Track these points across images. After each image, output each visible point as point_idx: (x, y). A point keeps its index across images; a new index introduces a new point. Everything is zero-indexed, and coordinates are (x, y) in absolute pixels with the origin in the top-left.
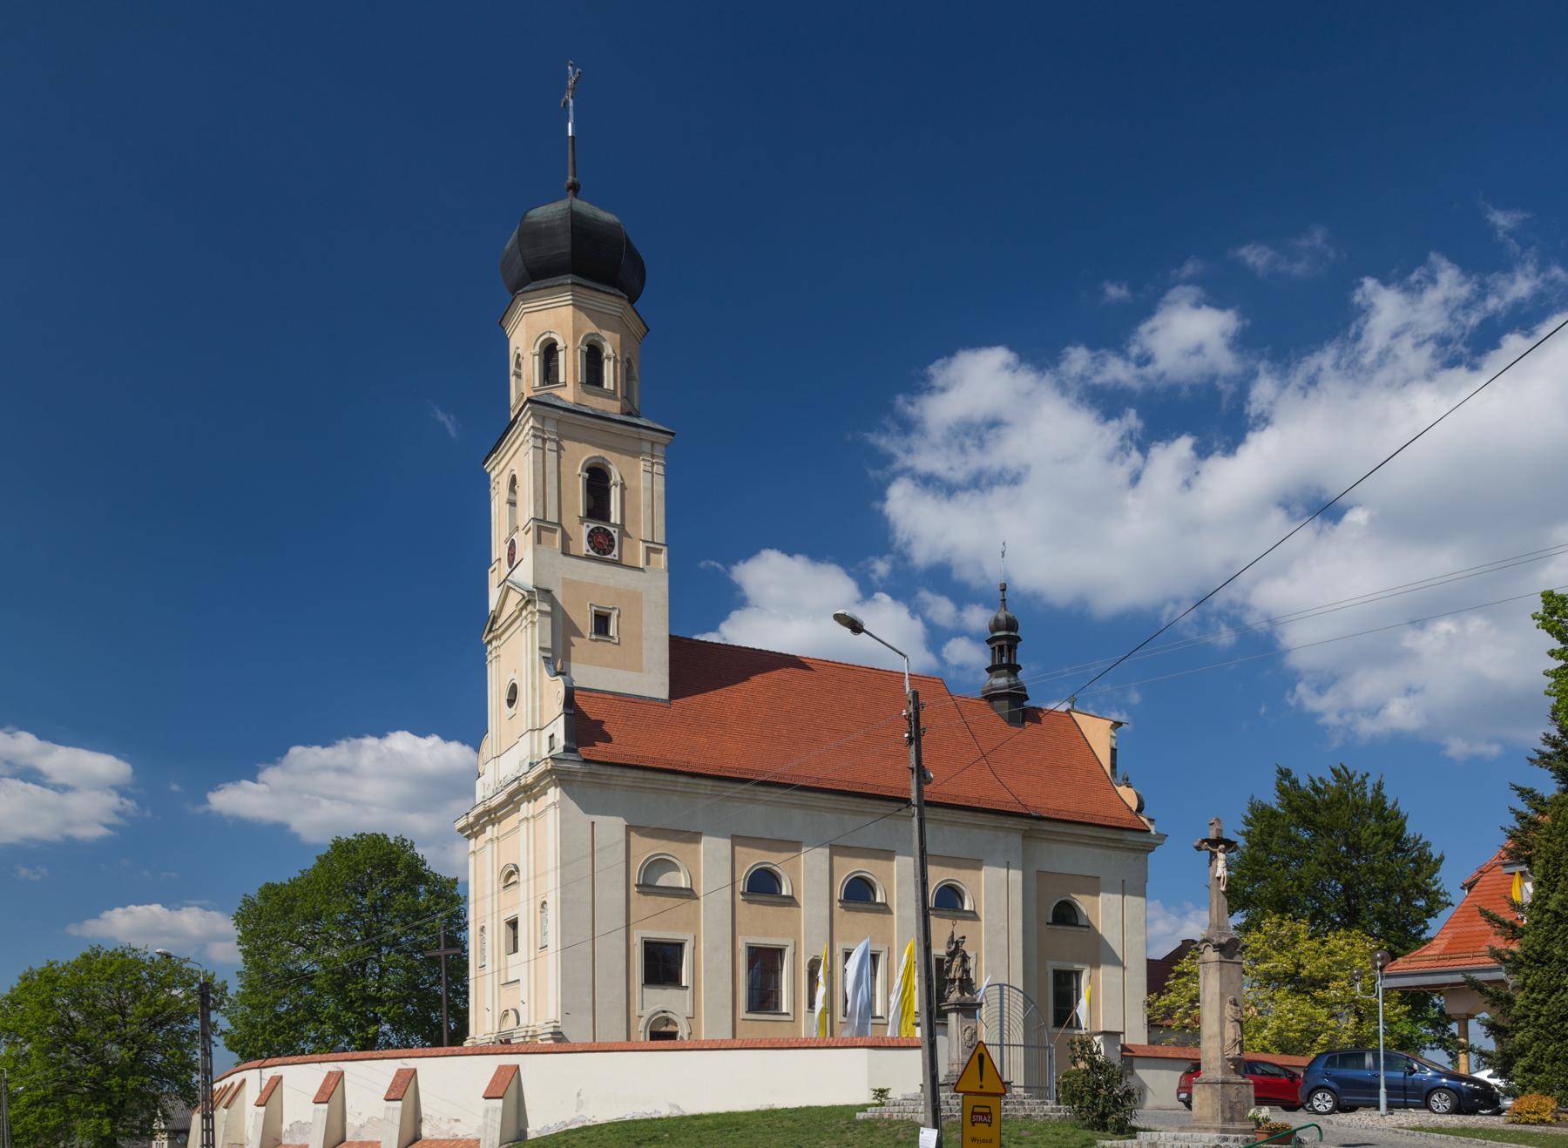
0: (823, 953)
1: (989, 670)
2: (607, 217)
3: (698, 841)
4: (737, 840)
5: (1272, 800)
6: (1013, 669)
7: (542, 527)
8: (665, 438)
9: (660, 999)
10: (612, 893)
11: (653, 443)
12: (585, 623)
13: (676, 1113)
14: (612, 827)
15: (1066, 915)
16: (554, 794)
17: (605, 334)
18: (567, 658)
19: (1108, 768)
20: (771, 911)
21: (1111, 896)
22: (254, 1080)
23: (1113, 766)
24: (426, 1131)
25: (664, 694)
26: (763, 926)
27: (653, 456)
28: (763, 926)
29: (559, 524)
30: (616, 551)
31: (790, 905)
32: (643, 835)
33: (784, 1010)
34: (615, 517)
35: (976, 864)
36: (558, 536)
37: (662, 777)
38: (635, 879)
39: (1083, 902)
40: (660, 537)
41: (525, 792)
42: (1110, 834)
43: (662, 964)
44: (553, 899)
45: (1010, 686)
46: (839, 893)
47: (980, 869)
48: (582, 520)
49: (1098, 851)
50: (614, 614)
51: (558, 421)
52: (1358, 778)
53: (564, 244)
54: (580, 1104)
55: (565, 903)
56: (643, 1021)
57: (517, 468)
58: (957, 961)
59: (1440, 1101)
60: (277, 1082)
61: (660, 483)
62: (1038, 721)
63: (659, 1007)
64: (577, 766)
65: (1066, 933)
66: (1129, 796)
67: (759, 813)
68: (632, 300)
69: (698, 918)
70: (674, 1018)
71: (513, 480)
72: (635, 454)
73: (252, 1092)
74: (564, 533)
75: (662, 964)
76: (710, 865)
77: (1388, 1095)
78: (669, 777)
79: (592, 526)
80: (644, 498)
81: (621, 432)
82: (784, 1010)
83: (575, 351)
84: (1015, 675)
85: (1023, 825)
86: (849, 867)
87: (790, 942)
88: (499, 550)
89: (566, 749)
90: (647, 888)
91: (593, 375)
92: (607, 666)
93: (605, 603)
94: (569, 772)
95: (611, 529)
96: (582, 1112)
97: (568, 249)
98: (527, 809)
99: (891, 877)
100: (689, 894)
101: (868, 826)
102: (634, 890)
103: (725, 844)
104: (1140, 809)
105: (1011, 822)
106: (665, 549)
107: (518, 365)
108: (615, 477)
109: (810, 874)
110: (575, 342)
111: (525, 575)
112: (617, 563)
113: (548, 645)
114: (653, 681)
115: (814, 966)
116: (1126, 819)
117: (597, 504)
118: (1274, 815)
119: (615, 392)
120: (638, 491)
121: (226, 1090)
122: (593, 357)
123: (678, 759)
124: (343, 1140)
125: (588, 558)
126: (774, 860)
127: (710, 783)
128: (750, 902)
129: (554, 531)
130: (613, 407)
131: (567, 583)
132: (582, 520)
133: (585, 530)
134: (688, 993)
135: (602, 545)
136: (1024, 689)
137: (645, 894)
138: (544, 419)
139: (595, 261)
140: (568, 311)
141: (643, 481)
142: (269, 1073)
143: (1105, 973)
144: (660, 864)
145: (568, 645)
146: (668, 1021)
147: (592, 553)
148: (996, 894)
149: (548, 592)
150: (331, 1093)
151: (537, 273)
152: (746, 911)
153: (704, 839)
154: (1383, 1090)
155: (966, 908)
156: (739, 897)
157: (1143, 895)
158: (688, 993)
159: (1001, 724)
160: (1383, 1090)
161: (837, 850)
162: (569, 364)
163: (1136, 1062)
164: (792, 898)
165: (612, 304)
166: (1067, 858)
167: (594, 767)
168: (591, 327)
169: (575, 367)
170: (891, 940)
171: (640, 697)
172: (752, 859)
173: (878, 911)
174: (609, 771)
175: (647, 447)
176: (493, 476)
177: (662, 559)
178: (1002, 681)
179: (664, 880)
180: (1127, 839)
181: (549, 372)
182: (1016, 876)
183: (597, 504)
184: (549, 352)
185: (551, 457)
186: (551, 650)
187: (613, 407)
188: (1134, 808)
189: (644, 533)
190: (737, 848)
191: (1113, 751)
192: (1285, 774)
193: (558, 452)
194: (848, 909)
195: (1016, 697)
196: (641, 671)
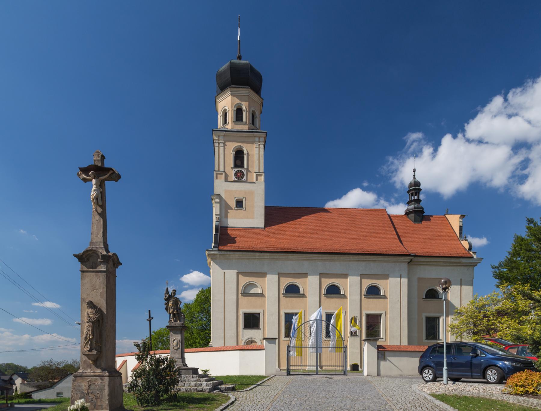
0: (357, 314)
2: (248, 62)
3: (265, 277)
5: (524, 233)
8: (264, 135)
12: (232, 203)
14: (231, 274)
15: (432, 294)
17: (243, 103)
18: (226, 217)
20: (376, 301)
23: (461, 233)
25: (263, 226)
27: (259, 142)
28: (291, 305)
29: (224, 171)
30: (245, 178)
31: (302, 297)
32: (244, 276)
34: (246, 167)
35: (385, 277)
36: (223, 176)
37: (249, 253)
38: (240, 291)
40: (262, 170)
42: (453, 260)
43: (251, 321)
45: (415, 208)
47: (387, 279)
48: (232, 169)
50: (244, 200)
51: (224, 136)
53: (229, 76)
56: (243, 342)
59: (492, 375)
61: (262, 151)
63: (249, 337)
64: (216, 253)
65: (432, 302)
66: (465, 244)
67: (291, 264)
68: (257, 90)
70: (255, 340)
72: (253, 143)
74: (226, 174)
75: (251, 321)
76: (270, 285)
77: (448, 371)
78: (252, 254)
79: (236, 170)
80: (256, 157)
85: (408, 259)
86: (327, 282)
90: (245, 294)
92: (242, 218)
93: (240, 196)
94: (214, 255)
95: (243, 170)
97: (230, 76)
99: (347, 284)
100: (261, 295)
101: (337, 265)
102: (240, 295)
103: (276, 277)
104: (470, 249)
105: (402, 259)
106: (263, 174)
108: (245, 152)
109: (311, 285)
112: (246, 182)
113: (219, 213)
116: (462, 253)
118: (522, 239)
119: (246, 122)
120: (253, 155)
122: (239, 112)
123: (264, 247)
125: (235, 181)
126: (298, 282)
127: (268, 254)
128: (286, 297)
129: (222, 174)
130: (245, 128)
131: (226, 191)
132: (232, 169)
133: (233, 172)
135: (240, 176)
136: (423, 208)
137: (244, 296)
138: (219, 136)
139: (242, 77)
140: (229, 98)
144: (251, 285)
145: (227, 213)
146: (252, 341)
147: (236, 180)
148: (396, 289)
149: (104, 158)
151: (223, 88)
152: (365, 300)
153: (267, 276)
154: (445, 368)
156: (282, 295)
157: (472, 284)
158: (261, 331)
159: (411, 223)
160: (445, 368)
161: (322, 275)
162: (230, 116)
163: (386, 353)
165: (246, 91)
167: (223, 252)
168: (237, 101)
169: (232, 116)
170: (387, 308)
171: (253, 228)
173: (341, 298)
174: (229, 253)
175: (257, 139)
178: (412, 207)
179: (252, 291)
180: (464, 261)
181: (225, 122)
182: (405, 281)
185: (222, 149)
186: (220, 215)
188: (467, 249)
191: (461, 228)
192: (531, 221)
193: (224, 147)
194: (327, 297)
196: (254, 218)
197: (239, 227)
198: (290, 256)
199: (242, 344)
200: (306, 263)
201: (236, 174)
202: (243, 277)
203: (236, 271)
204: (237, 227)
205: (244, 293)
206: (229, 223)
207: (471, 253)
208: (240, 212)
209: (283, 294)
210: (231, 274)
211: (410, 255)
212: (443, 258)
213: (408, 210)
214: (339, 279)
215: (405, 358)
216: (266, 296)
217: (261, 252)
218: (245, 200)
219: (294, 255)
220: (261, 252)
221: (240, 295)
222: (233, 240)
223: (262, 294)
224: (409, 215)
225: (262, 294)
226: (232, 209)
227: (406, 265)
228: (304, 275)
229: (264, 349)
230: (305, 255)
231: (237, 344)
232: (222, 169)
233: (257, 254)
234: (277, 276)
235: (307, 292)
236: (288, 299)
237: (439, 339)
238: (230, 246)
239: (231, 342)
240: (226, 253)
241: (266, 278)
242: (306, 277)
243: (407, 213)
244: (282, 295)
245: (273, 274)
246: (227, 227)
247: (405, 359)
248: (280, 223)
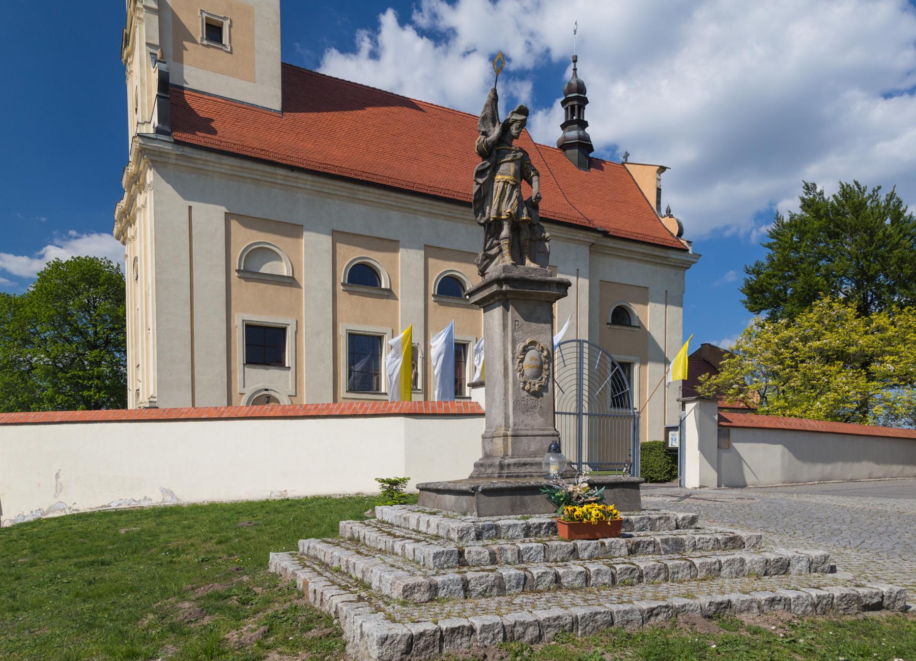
0: (418, 339)
3: (298, 236)
4: (338, 236)
6: (584, 125)
9: (263, 378)
10: (211, 277)
12: (197, 29)
13: (170, 502)
14: (210, 216)
18: (179, 59)
19: (654, 205)
21: (658, 305)
23: (658, 203)
25: (277, 105)
26: (361, 315)
28: (361, 315)
31: (388, 297)
33: (383, 391)
37: (261, 167)
38: (235, 265)
39: (636, 309)
42: (658, 252)
43: (265, 345)
45: (580, 138)
46: (433, 289)
49: (648, 267)
52: (869, 192)
54: (59, 488)
58: (506, 172)
62: (602, 168)
63: (261, 386)
64: (168, 147)
67: (360, 212)
69: (300, 305)
82: (383, 391)
84: (583, 129)
85: (591, 237)
89: (158, 131)
90: (249, 274)
92: (220, 72)
93: (218, 11)
94: (161, 153)
96: (61, 498)
100: (291, 282)
102: (234, 275)
103: (326, 241)
104: (680, 234)
105: (581, 235)
109: (406, 271)
113: (156, 42)
114: (267, 93)
126: (377, 259)
127: (309, 178)
134: (290, 374)
137: (247, 279)
143: (650, 367)
146: (269, 399)
152: (347, 301)
155: (383, 286)
156: (340, 288)
157: (680, 304)
158: (290, 374)
159: (572, 167)
163: (733, 432)
164: (390, 290)
166: (626, 271)
167: (188, 151)
170: (479, 330)
172: (350, 255)
173: (381, 297)
174: (204, 155)
179: (266, 269)
186: (161, 46)
188: (676, 233)
190: (338, 245)
194: (442, 304)
195: (584, 145)
197: (216, 96)
198: (362, 192)
199: (243, 401)
200: (395, 216)
202: (243, 229)
203: (224, 209)
204: (210, 95)
205: (245, 271)
206: (186, 78)
207: (685, 243)
208: (213, 52)
209: (343, 284)
210: (210, 216)
211: (594, 230)
212: (643, 246)
213: (565, 138)
214: (464, 265)
215: (761, 445)
216: (303, 285)
217: (292, 168)
218: (230, 26)
219: (371, 190)
220: (292, 168)
221: (234, 275)
222: (206, 125)
223: (293, 278)
224: (568, 151)
225: (293, 278)
226: (194, 41)
227: (585, 250)
228: (391, 245)
229: (482, 415)
230: (394, 195)
231: (229, 403)
233: (281, 171)
234: (329, 239)
235: (397, 287)
236: (355, 298)
237: (629, 406)
238: (200, 138)
239: (212, 396)
240: (196, 154)
241: (303, 241)
242: (396, 250)
243: (564, 146)
244: (340, 288)
245: (317, 231)
246: (183, 88)
247: (761, 446)
248: (318, 111)
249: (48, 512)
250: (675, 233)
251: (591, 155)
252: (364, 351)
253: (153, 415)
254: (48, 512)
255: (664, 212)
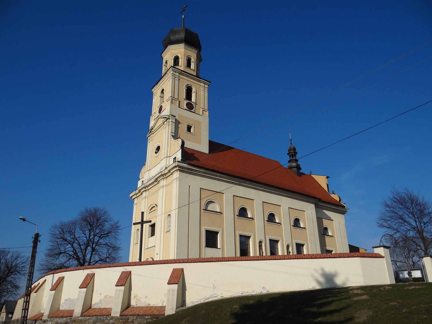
1: (289, 162)
7: (173, 99)
11: (205, 84)
16: (177, 175)
19: (327, 190)
22: (50, 279)
24: (133, 303)
25: (207, 152)
30: (194, 109)
36: (178, 102)
40: (206, 108)
41: (163, 176)
43: (211, 239)
44: (174, 215)
55: (179, 215)
57: (167, 84)
60: (61, 280)
71: (163, 91)
73: (48, 286)
79: (188, 102)
80: (202, 97)
81: (198, 77)
83: (184, 59)
87: (253, 234)
88: (155, 109)
91: (189, 65)
95: (193, 104)
98: (163, 183)
104: (340, 200)
105: (312, 200)
107: (166, 62)
110: (184, 56)
111: (166, 112)
113: (174, 132)
115: (260, 242)
117: (189, 96)
121: (35, 287)
124: (91, 308)
135: (190, 107)
139: (191, 41)
141: (202, 93)
142: (57, 276)
147: (187, 109)
150: (88, 283)
176: (154, 92)
177: (207, 113)
183: (189, 96)
184: (176, 59)
185: (177, 82)
187: (194, 73)
189: (202, 106)
191: (327, 185)
201: (187, 104)
211: (316, 198)
222: (197, 159)
229: (383, 257)
232: (176, 96)
238: (195, 162)
249: (209, 298)
250: (338, 200)
251: (301, 171)
252: (244, 241)
253: (283, 258)
254: (209, 298)
255: (331, 192)
